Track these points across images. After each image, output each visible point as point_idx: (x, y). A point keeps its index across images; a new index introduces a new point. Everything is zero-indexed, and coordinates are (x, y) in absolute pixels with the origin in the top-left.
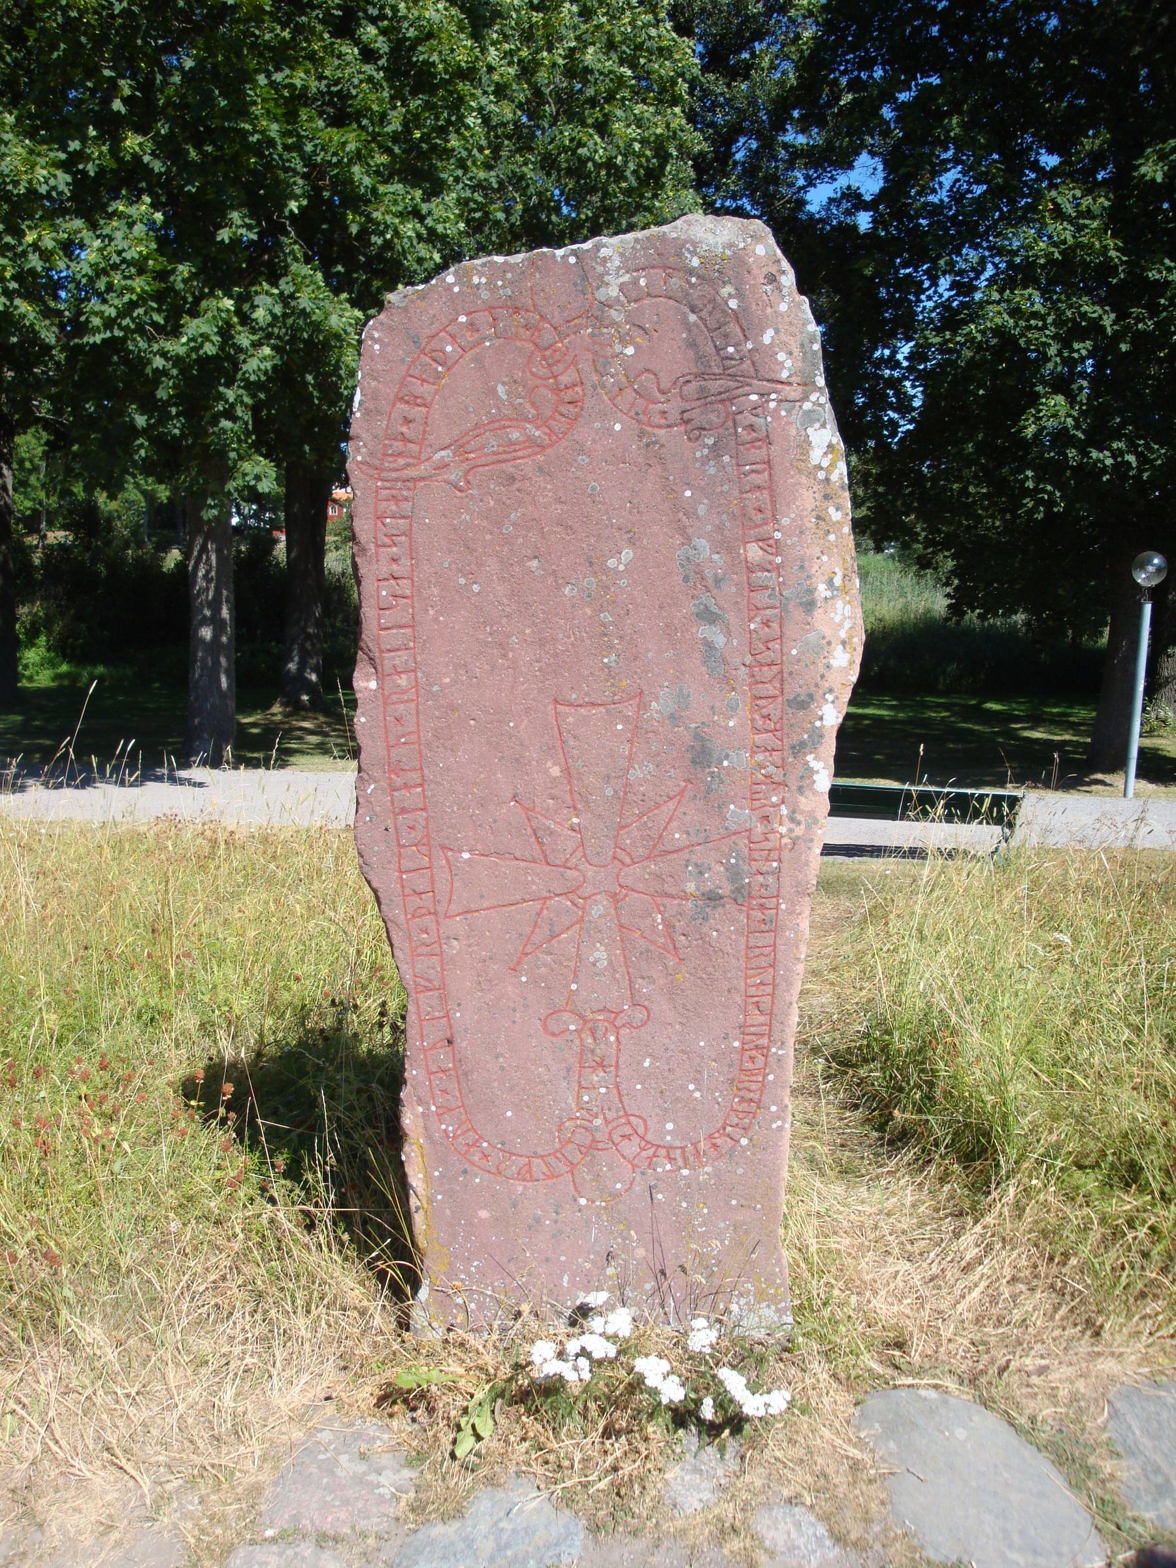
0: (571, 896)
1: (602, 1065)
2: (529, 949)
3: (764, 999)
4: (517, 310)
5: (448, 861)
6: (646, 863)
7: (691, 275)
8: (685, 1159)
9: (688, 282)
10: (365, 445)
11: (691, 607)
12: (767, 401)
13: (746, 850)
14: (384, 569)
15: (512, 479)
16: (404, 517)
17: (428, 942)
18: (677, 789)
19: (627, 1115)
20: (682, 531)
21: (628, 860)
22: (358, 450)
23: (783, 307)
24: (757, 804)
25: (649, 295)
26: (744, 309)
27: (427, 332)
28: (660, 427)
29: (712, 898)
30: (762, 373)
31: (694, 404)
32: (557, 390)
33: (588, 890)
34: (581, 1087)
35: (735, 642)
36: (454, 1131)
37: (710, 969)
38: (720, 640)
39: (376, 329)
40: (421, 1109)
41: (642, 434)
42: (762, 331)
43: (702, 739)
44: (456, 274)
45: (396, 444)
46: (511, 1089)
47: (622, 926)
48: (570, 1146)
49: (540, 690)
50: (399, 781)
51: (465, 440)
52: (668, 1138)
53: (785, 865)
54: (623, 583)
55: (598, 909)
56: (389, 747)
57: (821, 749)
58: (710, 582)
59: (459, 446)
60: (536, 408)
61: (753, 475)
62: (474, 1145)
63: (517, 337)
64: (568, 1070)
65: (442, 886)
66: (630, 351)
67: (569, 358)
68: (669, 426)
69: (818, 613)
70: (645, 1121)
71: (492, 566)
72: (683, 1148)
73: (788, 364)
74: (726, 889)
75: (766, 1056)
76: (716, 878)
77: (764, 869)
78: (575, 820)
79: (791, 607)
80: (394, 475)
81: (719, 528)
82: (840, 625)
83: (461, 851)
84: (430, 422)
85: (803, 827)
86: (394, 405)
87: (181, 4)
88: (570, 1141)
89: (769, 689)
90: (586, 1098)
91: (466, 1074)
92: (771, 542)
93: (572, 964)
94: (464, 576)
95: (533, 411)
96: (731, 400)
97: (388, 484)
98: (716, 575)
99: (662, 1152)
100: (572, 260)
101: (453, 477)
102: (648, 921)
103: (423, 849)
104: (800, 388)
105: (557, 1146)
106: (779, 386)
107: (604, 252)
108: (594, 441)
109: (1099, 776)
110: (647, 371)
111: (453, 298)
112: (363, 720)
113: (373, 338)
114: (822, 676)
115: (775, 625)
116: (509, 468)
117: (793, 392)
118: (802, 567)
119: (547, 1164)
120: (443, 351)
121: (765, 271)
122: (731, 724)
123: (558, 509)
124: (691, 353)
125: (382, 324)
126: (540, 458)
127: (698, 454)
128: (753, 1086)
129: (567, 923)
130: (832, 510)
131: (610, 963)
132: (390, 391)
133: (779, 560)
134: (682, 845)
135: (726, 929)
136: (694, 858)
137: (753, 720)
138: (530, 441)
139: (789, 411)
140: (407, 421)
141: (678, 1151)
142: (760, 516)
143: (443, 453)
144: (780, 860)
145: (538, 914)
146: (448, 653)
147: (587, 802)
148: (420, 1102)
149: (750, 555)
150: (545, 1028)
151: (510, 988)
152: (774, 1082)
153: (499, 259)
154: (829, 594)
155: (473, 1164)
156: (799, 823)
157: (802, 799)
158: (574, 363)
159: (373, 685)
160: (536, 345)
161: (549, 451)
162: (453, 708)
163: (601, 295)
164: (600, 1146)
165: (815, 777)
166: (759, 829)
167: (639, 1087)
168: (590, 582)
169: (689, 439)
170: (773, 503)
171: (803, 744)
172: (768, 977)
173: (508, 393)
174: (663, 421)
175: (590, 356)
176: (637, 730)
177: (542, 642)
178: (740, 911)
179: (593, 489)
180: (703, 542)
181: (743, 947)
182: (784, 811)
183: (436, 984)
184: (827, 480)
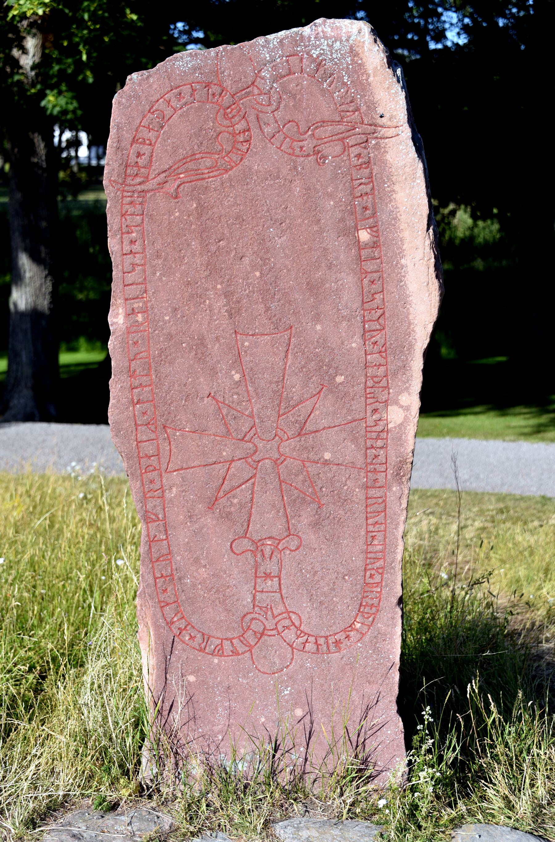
87: (5, 200)
91: (180, 579)
109: (11, 329)
146: (168, 300)
161: (230, 172)
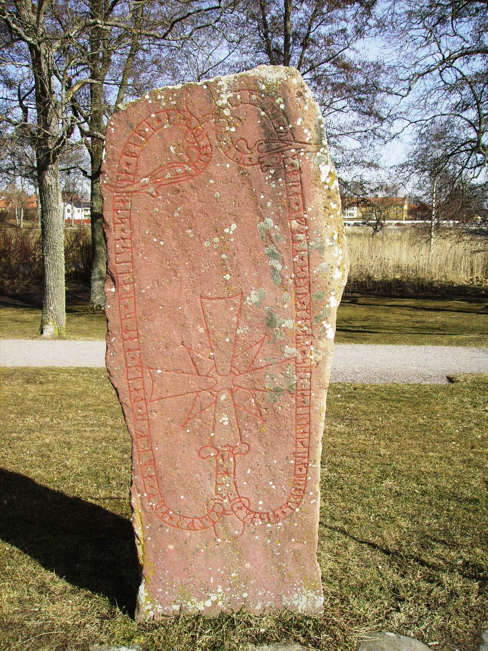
1: (227, 473)
2: (190, 416)
3: (305, 440)
5: (151, 374)
6: (246, 374)
8: (269, 519)
12: (300, 152)
18: (260, 339)
21: (237, 373)
24: (299, 345)
25: (241, 102)
28: (248, 165)
30: (296, 139)
32: (199, 148)
33: (219, 387)
34: (217, 484)
35: (286, 267)
36: (156, 506)
38: (279, 267)
40: (139, 495)
41: (239, 169)
45: (122, 175)
52: (260, 508)
54: (232, 240)
56: (121, 320)
59: (153, 176)
62: (165, 513)
63: (179, 123)
64: (211, 475)
65: (148, 387)
68: (252, 165)
69: (326, 253)
71: (169, 232)
73: (309, 134)
78: (212, 354)
82: (337, 259)
85: (321, 356)
90: (219, 489)
91: (161, 478)
94: (156, 237)
97: (119, 194)
99: (258, 515)
100: (205, 87)
102: (248, 402)
103: (139, 368)
104: (315, 146)
107: (220, 83)
110: (242, 139)
114: (329, 283)
115: (306, 259)
121: (297, 90)
122: (285, 307)
123: (200, 205)
124: (263, 130)
127: (267, 178)
128: (301, 483)
130: (332, 204)
131: (230, 423)
133: (307, 228)
134: (263, 365)
136: (269, 372)
141: (265, 515)
142: (297, 207)
143: (145, 179)
145: (195, 399)
148: (139, 492)
150: (199, 454)
151: (181, 436)
152: (311, 480)
154: (331, 244)
155: (165, 522)
160: (189, 127)
162: (152, 300)
163: (220, 103)
165: (327, 332)
167: (245, 483)
168: (216, 240)
169: (262, 171)
170: (304, 201)
173: (175, 150)
180: (270, 220)
181: (294, 414)
184: (329, 189)
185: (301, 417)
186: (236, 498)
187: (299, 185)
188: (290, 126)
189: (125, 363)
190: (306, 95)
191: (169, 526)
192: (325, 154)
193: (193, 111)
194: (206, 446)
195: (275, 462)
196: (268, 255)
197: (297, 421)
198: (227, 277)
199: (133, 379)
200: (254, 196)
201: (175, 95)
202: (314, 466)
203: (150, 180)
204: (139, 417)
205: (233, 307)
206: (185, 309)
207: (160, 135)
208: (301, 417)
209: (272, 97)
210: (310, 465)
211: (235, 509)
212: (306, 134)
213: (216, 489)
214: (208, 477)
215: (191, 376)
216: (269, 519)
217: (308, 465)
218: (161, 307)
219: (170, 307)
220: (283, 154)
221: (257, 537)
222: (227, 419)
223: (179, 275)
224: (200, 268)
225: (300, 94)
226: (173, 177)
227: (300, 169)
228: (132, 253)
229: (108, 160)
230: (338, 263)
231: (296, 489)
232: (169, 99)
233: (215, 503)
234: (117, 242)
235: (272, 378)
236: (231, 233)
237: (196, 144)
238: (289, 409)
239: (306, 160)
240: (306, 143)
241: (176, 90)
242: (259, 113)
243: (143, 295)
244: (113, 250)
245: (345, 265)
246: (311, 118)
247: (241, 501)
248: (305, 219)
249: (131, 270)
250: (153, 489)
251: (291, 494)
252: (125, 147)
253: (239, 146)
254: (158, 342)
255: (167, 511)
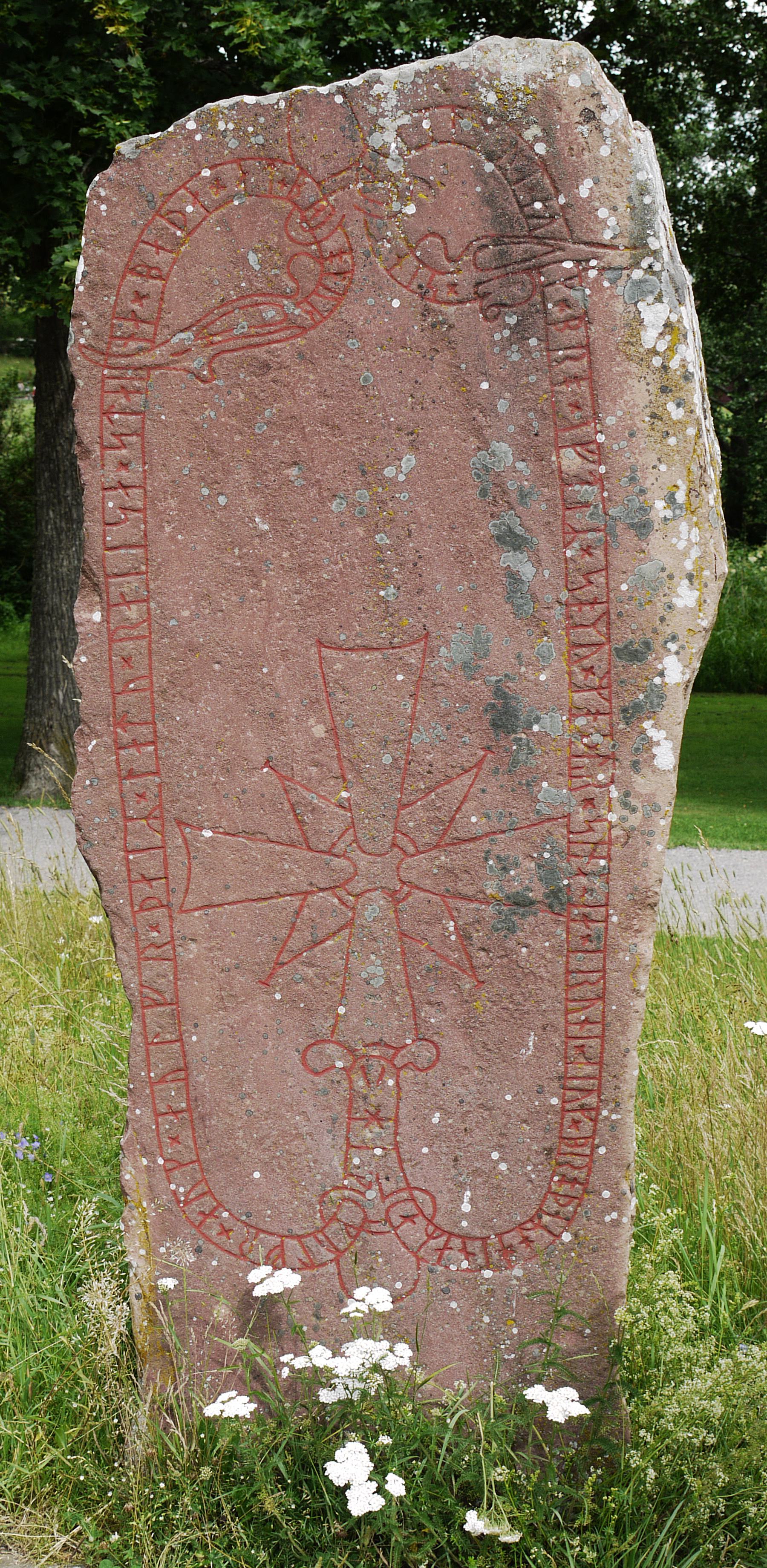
0: (342, 893)
1: (376, 1117)
2: (285, 957)
3: (592, 1042)
4: (272, 161)
5: (185, 840)
6: (434, 853)
7: (487, 114)
8: (487, 1255)
9: (484, 123)
10: (89, 326)
11: (491, 527)
12: (586, 270)
13: (564, 842)
14: (112, 475)
15: (266, 366)
16: (134, 413)
17: (159, 942)
18: (474, 760)
19: (410, 1188)
20: (478, 432)
21: (411, 849)
22: (80, 331)
23: (605, 151)
24: (578, 782)
25: (433, 139)
26: (554, 155)
27: (164, 189)
28: (449, 303)
29: (520, 903)
30: (578, 233)
31: (491, 274)
32: (320, 258)
33: (359, 885)
34: (349, 1146)
35: (547, 573)
36: (186, 1194)
37: (518, 998)
38: (527, 571)
39: (103, 186)
40: (145, 1162)
41: (426, 312)
42: (578, 180)
43: (505, 696)
44: (198, 119)
45: (126, 324)
46: (260, 1141)
47: (403, 934)
48: (335, 1225)
49: (301, 629)
50: (126, 737)
51: (209, 319)
52: (464, 1224)
53: (615, 864)
54: (404, 496)
55: (375, 907)
56: (114, 694)
57: (663, 714)
58: (514, 496)
59: (201, 327)
60: (295, 281)
61: (568, 363)
62: (211, 1214)
63: (271, 194)
64: (334, 1121)
65: (177, 871)
66: (411, 209)
67: (335, 219)
68: (460, 302)
69: (655, 538)
70: (433, 1198)
71: (242, 474)
72: (484, 1239)
73: (612, 221)
74: (537, 892)
75: (595, 1120)
76: (525, 878)
77: (588, 868)
78: (344, 794)
79: (620, 528)
80: (123, 361)
81: (523, 430)
82: (685, 554)
83: (201, 828)
84: (166, 297)
85: (639, 814)
86: (124, 277)
88: (334, 1218)
89: (593, 635)
90: (356, 1161)
91: (202, 1118)
92: (593, 447)
93: (339, 980)
94: (208, 485)
95: (292, 284)
96: (539, 268)
97: (116, 373)
98: (521, 489)
99: (456, 1242)
100: (339, 99)
101: (195, 365)
102: (438, 930)
103: (156, 823)
104: (628, 253)
105: (319, 1223)
106: (601, 250)
107: (377, 89)
108: (366, 320)
110: (434, 234)
111: (194, 148)
112: (84, 659)
113: (99, 197)
114: (662, 619)
115: (599, 553)
116: (261, 353)
117: (620, 258)
118: (632, 479)
119: (306, 1249)
120: (182, 212)
121: (580, 106)
122: (543, 677)
123: (322, 404)
124: (488, 211)
125: (109, 180)
126: (301, 341)
127: (497, 337)
128: (578, 1161)
129: (334, 927)
130: (671, 406)
131: (388, 981)
132: (119, 261)
133: (602, 469)
134: (480, 832)
135: (540, 942)
136: (496, 850)
137: (570, 674)
138: (289, 321)
139: (613, 282)
140: (139, 297)
141: (478, 1244)
142: (578, 414)
143: (182, 335)
144: (609, 858)
145: (297, 913)
147: (359, 772)
148: (145, 1152)
149: (565, 463)
150: (304, 1062)
151: (260, 1007)
152: (606, 1157)
153: (250, 99)
154: (669, 513)
155: (208, 1239)
156: (634, 810)
157: (638, 779)
158: (341, 225)
159: (97, 617)
160: (295, 204)
162: (192, 648)
163: (376, 140)
164: (374, 1227)
165: (655, 750)
166: (582, 815)
167: (425, 1150)
168: (363, 495)
169: (486, 318)
170: (594, 397)
171: (638, 707)
172: (595, 1011)
173: (261, 263)
174: (452, 296)
175: (362, 216)
176: (421, 682)
177: (302, 570)
178: (557, 922)
179: (366, 380)
180: (504, 446)
181: (561, 970)
182: (614, 793)
183: (168, 997)
184: (665, 368)
185: (581, 977)
186: (400, 1190)
187: (581, 357)
188: (562, 200)
189: (119, 806)
190: (605, 118)
191: (219, 1252)
192: (654, 273)
193: (305, 161)
194: (324, 1041)
195: (508, 1097)
196: (498, 538)
197: (569, 987)
198: (389, 592)
199: (139, 851)
200: (462, 384)
201: (262, 120)
202: (614, 1117)
203: (196, 337)
204: (151, 952)
205: (402, 672)
206: (279, 673)
207: (220, 222)
208: (581, 977)
209: (513, 124)
210: (605, 1113)
211: (396, 1220)
212: (604, 221)
213: (347, 1160)
214: (326, 1125)
215: (291, 849)
216: (487, 1255)
217: (598, 1114)
218: (217, 667)
219: (240, 667)
220: (541, 274)
221: (454, 1305)
222: (380, 971)
223: (264, 583)
224: (317, 566)
225: (589, 116)
226: (253, 331)
227: (586, 313)
228: (145, 523)
229: (92, 287)
230: (689, 565)
231: (564, 1179)
232: (245, 132)
233: (344, 1199)
234: (107, 493)
235: (504, 869)
236: (402, 478)
237: (314, 247)
238: (549, 956)
239: (602, 289)
240: (605, 246)
241: (263, 107)
242: (479, 165)
243: (169, 632)
244: (98, 515)
245: (706, 573)
246: (616, 178)
247: (413, 1199)
248: (599, 446)
249: (143, 568)
250: (180, 1147)
251: (549, 1191)
252: (133, 251)
253: (425, 251)
254: (208, 756)
255: (215, 1209)
